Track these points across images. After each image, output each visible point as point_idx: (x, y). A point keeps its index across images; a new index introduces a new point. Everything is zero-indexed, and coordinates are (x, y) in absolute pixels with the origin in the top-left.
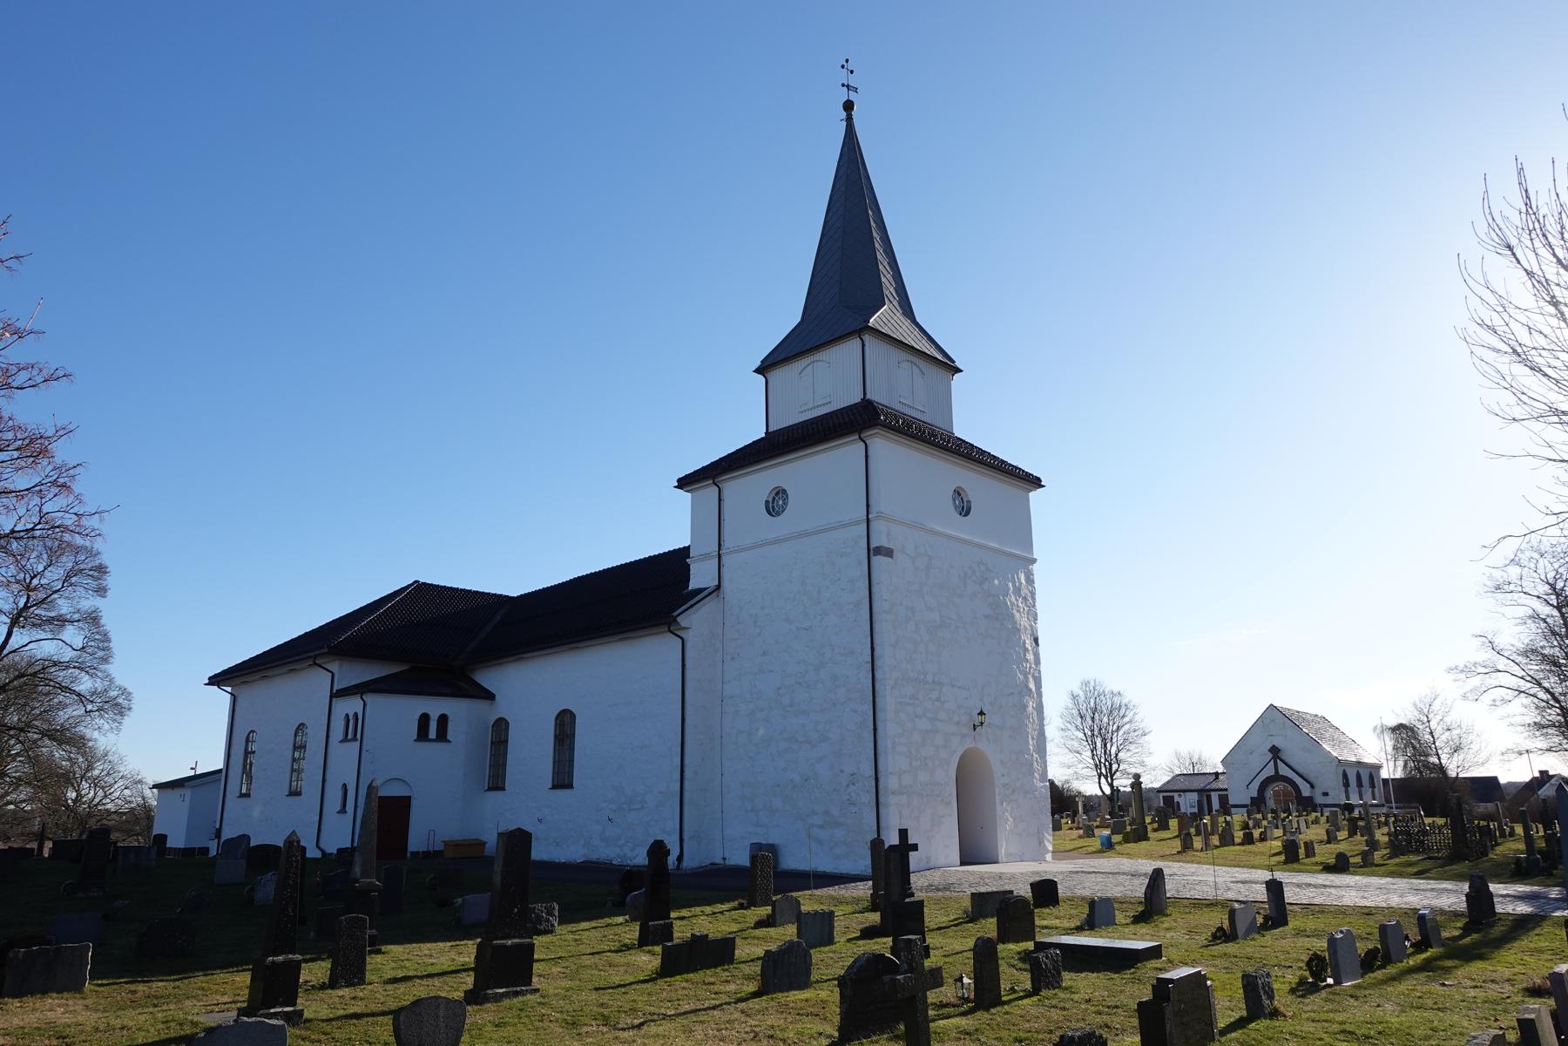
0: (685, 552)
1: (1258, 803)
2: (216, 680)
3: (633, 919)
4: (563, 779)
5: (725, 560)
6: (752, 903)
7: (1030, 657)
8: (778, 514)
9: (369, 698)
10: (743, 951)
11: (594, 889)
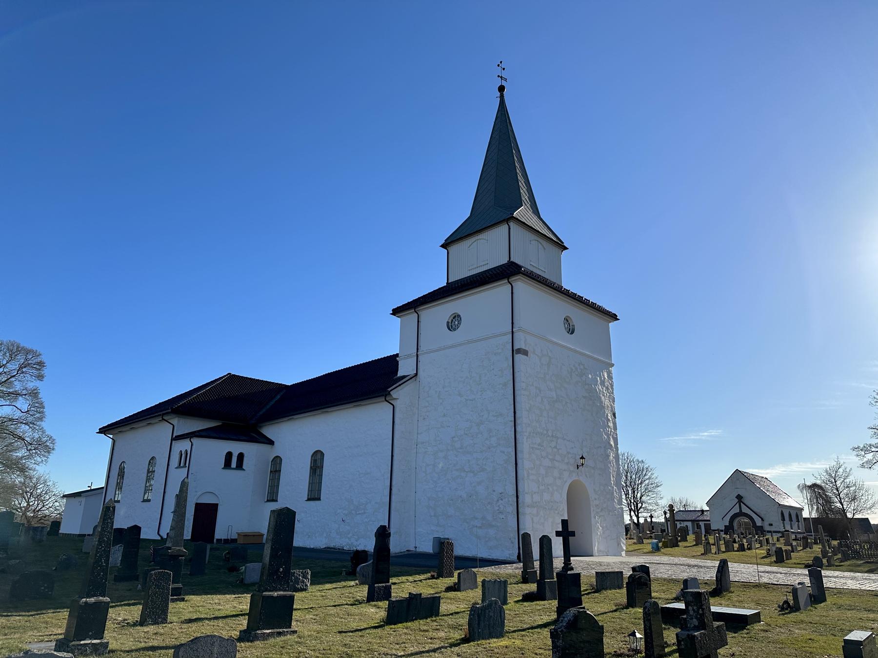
0: (397, 355)
1: (729, 529)
2: (104, 431)
3: (362, 583)
4: (314, 495)
5: (420, 358)
6: (440, 575)
7: (611, 424)
8: (455, 330)
9: (195, 441)
10: (445, 607)
11: (335, 565)
